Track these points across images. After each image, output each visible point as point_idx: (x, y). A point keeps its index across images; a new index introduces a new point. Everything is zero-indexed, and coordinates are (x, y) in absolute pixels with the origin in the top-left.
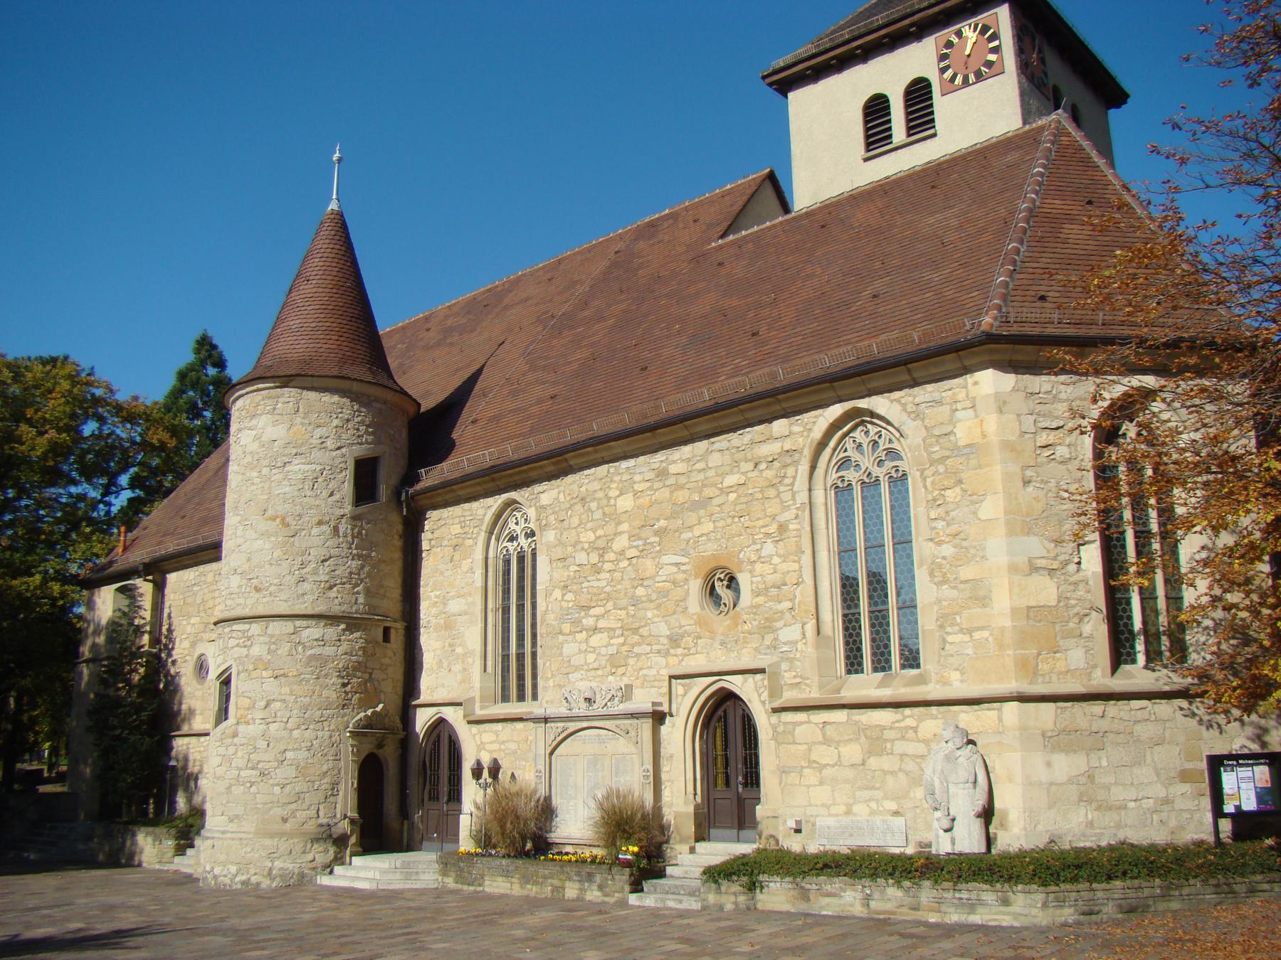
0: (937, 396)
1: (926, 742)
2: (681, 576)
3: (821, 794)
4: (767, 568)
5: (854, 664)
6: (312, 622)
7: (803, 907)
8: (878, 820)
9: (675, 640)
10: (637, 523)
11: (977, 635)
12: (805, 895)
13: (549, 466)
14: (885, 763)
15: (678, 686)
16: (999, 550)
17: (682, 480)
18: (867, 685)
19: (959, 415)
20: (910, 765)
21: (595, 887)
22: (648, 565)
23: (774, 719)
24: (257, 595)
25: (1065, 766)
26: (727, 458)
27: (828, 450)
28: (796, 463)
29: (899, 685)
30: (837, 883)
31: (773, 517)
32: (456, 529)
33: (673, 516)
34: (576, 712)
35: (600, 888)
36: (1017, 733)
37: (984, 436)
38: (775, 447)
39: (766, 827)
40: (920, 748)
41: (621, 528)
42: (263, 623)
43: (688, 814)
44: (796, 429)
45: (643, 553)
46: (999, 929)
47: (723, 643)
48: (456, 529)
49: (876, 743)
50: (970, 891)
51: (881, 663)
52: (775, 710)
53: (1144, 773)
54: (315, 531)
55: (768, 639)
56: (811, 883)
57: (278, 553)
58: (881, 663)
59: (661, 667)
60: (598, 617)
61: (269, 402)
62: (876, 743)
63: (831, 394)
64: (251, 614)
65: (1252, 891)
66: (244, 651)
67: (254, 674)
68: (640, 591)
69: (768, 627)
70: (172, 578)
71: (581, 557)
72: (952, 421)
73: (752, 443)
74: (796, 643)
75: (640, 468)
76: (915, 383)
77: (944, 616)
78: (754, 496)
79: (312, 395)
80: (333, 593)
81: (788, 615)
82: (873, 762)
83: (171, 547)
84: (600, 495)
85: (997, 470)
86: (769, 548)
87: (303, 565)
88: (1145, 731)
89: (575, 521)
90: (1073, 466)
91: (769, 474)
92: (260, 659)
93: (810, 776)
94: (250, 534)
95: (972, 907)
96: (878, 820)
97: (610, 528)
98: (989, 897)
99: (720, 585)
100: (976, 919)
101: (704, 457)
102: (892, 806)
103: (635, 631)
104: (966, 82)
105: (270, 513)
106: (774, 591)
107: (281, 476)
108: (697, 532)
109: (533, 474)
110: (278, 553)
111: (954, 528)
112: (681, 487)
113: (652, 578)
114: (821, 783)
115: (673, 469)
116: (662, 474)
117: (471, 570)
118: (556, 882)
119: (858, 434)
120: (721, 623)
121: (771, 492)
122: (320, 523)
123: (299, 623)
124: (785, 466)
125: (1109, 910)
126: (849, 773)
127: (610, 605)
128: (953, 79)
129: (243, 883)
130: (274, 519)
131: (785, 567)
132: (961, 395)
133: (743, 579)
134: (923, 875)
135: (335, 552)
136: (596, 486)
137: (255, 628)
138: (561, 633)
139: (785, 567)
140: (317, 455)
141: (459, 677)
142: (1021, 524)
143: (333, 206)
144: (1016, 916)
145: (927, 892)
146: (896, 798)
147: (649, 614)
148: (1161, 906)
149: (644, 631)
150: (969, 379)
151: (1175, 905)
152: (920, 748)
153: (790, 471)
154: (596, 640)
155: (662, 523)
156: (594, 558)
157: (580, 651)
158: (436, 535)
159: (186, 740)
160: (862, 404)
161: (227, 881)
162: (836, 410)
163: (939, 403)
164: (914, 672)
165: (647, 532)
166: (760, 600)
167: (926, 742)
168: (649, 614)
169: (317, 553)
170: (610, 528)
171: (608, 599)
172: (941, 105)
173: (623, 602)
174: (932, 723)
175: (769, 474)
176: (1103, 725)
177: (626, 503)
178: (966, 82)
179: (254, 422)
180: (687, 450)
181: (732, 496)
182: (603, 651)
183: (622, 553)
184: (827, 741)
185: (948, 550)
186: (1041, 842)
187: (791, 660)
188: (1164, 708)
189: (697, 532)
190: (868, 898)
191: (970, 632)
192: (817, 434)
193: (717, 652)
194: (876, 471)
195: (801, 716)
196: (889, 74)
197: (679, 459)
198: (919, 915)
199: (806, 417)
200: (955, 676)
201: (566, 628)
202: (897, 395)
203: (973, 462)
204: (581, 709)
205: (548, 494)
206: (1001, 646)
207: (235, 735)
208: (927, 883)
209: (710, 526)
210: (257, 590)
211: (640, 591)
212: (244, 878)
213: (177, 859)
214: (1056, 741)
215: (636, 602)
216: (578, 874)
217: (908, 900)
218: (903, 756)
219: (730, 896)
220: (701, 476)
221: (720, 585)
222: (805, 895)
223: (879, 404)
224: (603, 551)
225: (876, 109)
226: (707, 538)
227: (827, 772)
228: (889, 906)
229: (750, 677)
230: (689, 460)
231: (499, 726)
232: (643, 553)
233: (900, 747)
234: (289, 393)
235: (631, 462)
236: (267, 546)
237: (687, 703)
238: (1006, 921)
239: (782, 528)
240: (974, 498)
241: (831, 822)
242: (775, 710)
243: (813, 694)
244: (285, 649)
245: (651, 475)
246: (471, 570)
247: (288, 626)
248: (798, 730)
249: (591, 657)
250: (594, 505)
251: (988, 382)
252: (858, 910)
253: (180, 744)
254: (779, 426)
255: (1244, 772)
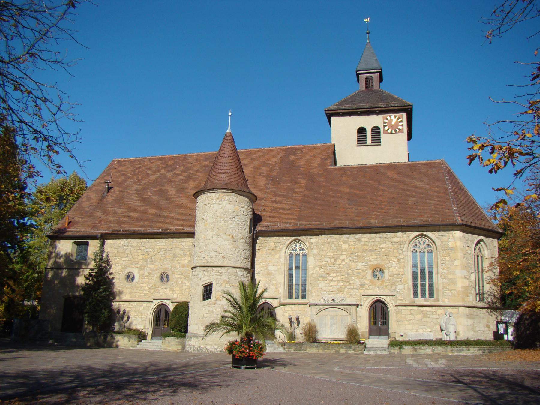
0: (444, 235)
1: (439, 315)
2: (365, 269)
3: (410, 327)
4: (394, 270)
5: (415, 295)
6: (241, 270)
7: (415, 353)
8: (425, 333)
9: (362, 286)
10: (349, 253)
11: (452, 291)
12: (416, 350)
13: (317, 232)
14: (428, 320)
15: (364, 298)
16: (459, 273)
17: (366, 243)
18: (420, 300)
19: (450, 240)
20: (434, 320)
21: (352, 350)
22: (354, 265)
23: (396, 308)
24: (223, 259)
25: (470, 322)
26: (382, 240)
27: (412, 242)
28: (404, 244)
29: (430, 301)
30: (425, 347)
31: (396, 257)
32: (273, 245)
33: (363, 252)
34: (327, 303)
35: (354, 350)
36: (117, 326)
37: (456, 246)
38: (398, 239)
39: (392, 335)
40: (438, 317)
41: (343, 253)
42: (226, 269)
43: (366, 332)
44: (405, 236)
45: (351, 261)
46: (466, 356)
47: (378, 288)
48: (273, 245)
49: (425, 315)
50: (459, 348)
51: (423, 295)
52: (396, 306)
53: (481, 325)
54: (241, 241)
55: (394, 288)
56: (418, 347)
57: (231, 247)
58: (423, 295)
59: (359, 293)
60: (334, 277)
61: (227, 197)
62: (425, 315)
63: (417, 229)
64: (222, 265)
65: (506, 349)
66: (219, 277)
67: (223, 285)
68: (350, 271)
69: (393, 284)
70: (106, 241)
71: (328, 260)
72: (448, 241)
73: (391, 237)
74: (402, 289)
75: (352, 238)
76: (439, 231)
77: (444, 286)
78: (397, 252)
79: (241, 197)
80: (245, 261)
81: (400, 282)
82: (424, 319)
83: (111, 231)
84: (336, 243)
85: (460, 255)
86: (394, 265)
87: (238, 251)
88: (482, 315)
89: (325, 249)
90: (471, 255)
91: (395, 246)
92: (225, 280)
93: (406, 323)
94: (220, 239)
95: (460, 351)
96: (425, 333)
97: (339, 253)
98: (465, 349)
99: (378, 271)
100: (461, 354)
101: (374, 238)
102: (430, 330)
103: (348, 282)
104: (392, 132)
105: (228, 233)
106: (395, 276)
107: (232, 222)
108: (371, 257)
109: (309, 233)
110: (231, 247)
111: (447, 266)
112: (366, 245)
113: (355, 268)
114: (409, 324)
115: (363, 240)
116: (359, 240)
117: (280, 258)
118: (337, 349)
119: (420, 240)
120: (378, 283)
121: (396, 251)
122: (243, 238)
123: (238, 270)
124: (400, 245)
125: (487, 352)
126: (418, 322)
127: (338, 274)
128: (388, 130)
129: (220, 351)
130: (230, 235)
131: (399, 270)
132: (451, 236)
133: (386, 272)
134: (448, 345)
135: (246, 248)
136: (334, 240)
137: (223, 270)
138: (319, 280)
139: (399, 270)
140: (241, 216)
141: (274, 290)
142: (465, 267)
143: (228, 131)
144: (471, 353)
145: (449, 348)
146: (431, 328)
147: (353, 278)
148: (494, 352)
149: (351, 282)
150: (453, 232)
151: (496, 352)
152: (438, 317)
153: (402, 246)
154: (332, 283)
155: (359, 254)
156: (333, 260)
157: (326, 286)
158: (262, 245)
159: (117, 303)
160: (425, 233)
161: (214, 350)
162: (417, 233)
163: (445, 236)
164: (432, 299)
165: (352, 256)
166: (391, 277)
167: (439, 315)
168: (353, 278)
169: (241, 248)
170: (339, 253)
171: (338, 272)
172: (383, 136)
173: (344, 274)
174: (441, 311)
175: (395, 246)
176: (475, 314)
177: (345, 246)
178: (392, 132)
179: (220, 202)
180: (369, 235)
181: (383, 250)
182: (335, 287)
183: (343, 260)
184: (411, 314)
185: (446, 271)
186: (466, 339)
187: (400, 294)
188: (484, 311)
189: (371, 257)
190: (434, 350)
191: (451, 290)
192: (411, 238)
193: (377, 290)
194: (424, 249)
195: (404, 308)
196: (369, 122)
197: (365, 237)
198: (447, 353)
199: (408, 233)
200: (446, 300)
201: (321, 279)
202: (434, 232)
203: (453, 252)
204: (330, 302)
205: (314, 239)
206: (459, 295)
207: (215, 304)
208: (449, 346)
209: (376, 257)
210: (223, 257)
211: (350, 271)
212: (221, 349)
213: (138, 346)
214: (470, 317)
215: (348, 274)
216: (346, 346)
217: (444, 350)
218: (432, 318)
219: (395, 351)
220: (373, 243)
221: (378, 271)
222: (416, 350)
223: (429, 234)
224: (336, 259)
225: (362, 131)
226: (375, 260)
227: (411, 321)
228: (439, 352)
229: (388, 297)
230: (369, 238)
231: (293, 306)
232: (351, 261)
233: (432, 316)
234: (234, 195)
235: (348, 235)
236: (227, 244)
237: (367, 303)
238: (469, 354)
239: (399, 260)
240: (453, 260)
241: (412, 334)
242: (396, 306)
243: (407, 302)
244: (233, 277)
245: (356, 240)
246: (280, 258)
247: (234, 270)
248: (403, 311)
249: (330, 288)
250: (333, 245)
251: (458, 234)
252: (431, 353)
253: (115, 305)
254: (399, 234)
255: (502, 325)
